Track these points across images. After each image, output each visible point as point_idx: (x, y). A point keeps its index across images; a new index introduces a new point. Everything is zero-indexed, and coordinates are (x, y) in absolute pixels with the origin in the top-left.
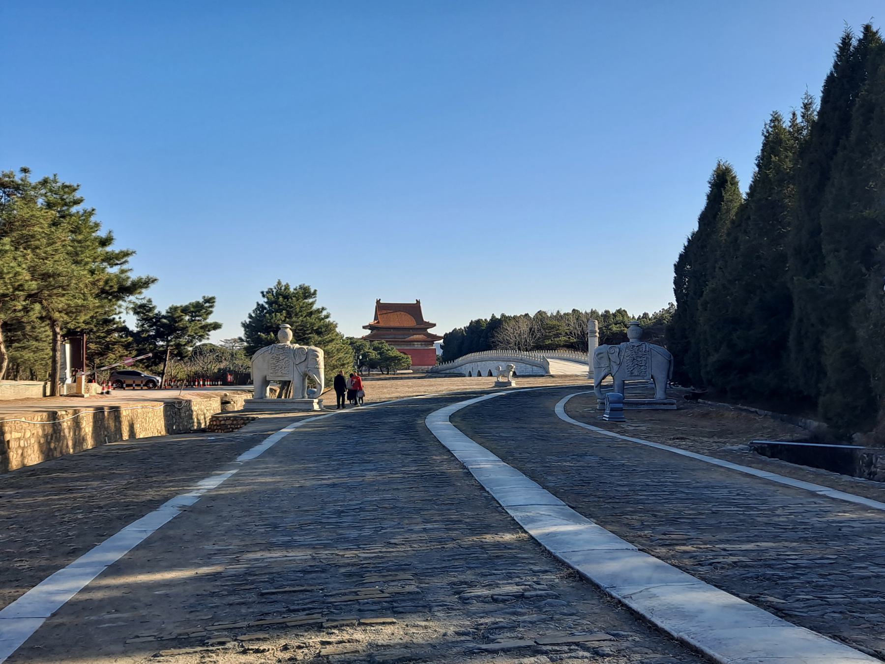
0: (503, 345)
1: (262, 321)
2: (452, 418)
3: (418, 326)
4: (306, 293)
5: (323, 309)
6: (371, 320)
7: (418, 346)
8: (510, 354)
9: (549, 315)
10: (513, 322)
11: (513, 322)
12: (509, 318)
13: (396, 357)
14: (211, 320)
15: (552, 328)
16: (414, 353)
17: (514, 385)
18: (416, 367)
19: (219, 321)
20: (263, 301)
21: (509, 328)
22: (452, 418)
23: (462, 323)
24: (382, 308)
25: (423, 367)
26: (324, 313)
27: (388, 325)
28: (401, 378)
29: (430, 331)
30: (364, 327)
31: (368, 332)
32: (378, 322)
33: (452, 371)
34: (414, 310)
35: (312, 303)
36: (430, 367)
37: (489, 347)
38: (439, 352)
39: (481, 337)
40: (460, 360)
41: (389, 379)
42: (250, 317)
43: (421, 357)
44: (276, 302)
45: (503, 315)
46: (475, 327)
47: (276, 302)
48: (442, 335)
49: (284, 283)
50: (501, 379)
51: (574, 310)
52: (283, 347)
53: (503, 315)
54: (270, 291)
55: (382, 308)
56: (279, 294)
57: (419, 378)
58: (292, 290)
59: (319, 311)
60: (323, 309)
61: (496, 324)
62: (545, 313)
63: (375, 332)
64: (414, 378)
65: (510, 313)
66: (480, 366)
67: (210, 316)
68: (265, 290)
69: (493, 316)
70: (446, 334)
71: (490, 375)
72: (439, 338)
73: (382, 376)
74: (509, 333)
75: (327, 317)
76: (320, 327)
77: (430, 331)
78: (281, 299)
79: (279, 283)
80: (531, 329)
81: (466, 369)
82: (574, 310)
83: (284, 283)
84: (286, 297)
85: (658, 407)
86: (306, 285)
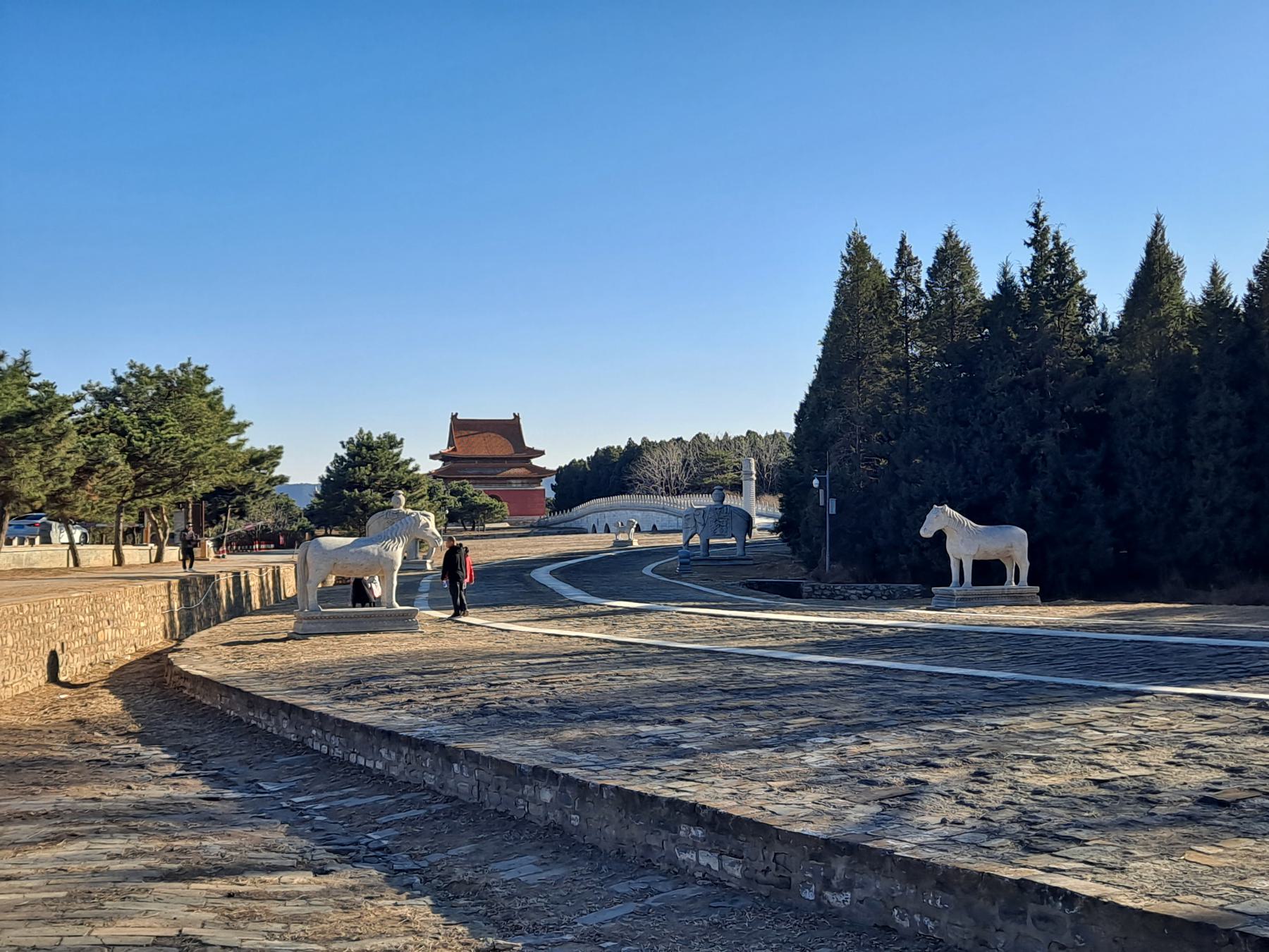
0: (642, 486)
1: (344, 476)
2: (551, 573)
3: (517, 455)
4: (392, 442)
5: (411, 460)
6: (443, 447)
7: (516, 486)
8: (648, 500)
9: (713, 438)
10: (658, 451)
11: (658, 451)
12: (653, 445)
13: (485, 506)
14: (277, 472)
15: (713, 460)
16: (510, 497)
17: (635, 544)
18: (514, 519)
19: (286, 474)
20: (343, 452)
21: (652, 459)
22: (551, 573)
23: (584, 452)
24: (460, 427)
25: (526, 518)
26: (411, 467)
27: (469, 454)
28: (494, 537)
29: (535, 462)
30: (433, 457)
31: (438, 464)
32: (455, 450)
33: (568, 525)
34: (511, 429)
35: (398, 454)
36: (537, 518)
37: (623, 489)
38: (551, 495)
39: (610, 474)
40: (580, 509)
41: (477, 537)
42: (328, 470)
43: (522, 503)
44: (358, 454)
45: (645, 441)
46: (603, 458)
47: (358, 454)
48: (555, 468)
49: (366, 432)
50: (622, 537)
51: (749, 432)
52: (397, 513)
53: (645, 441)
54: (351, 441)
55: (460, 427)
56: (360, 445)
57: (520, 536)
58: (375, 439)
59: (407, 462)
60: (411, 460)
61: (633, 453)
62: (706, 436)
63: (449, 464)
64: (513, 535)
65: (655, 438)
66: (608, 518)
67: (277, 469)
68: (346, 440)
69: (630, 442)
70: (560, 468)
71: (608, 530)
72: (550, 473)
73: (465, 534)
74: (654, 467)
75: (416, 469)
76: (409, 482)
77: (535, 462)
78: (364, 450)
79: (361, 431)
80: (684, 461)
81: (587, 522)
82: (749, 432)
83: (366, 432)
84: (369, 448)
85: (496, 533)
86: (392, 433)
